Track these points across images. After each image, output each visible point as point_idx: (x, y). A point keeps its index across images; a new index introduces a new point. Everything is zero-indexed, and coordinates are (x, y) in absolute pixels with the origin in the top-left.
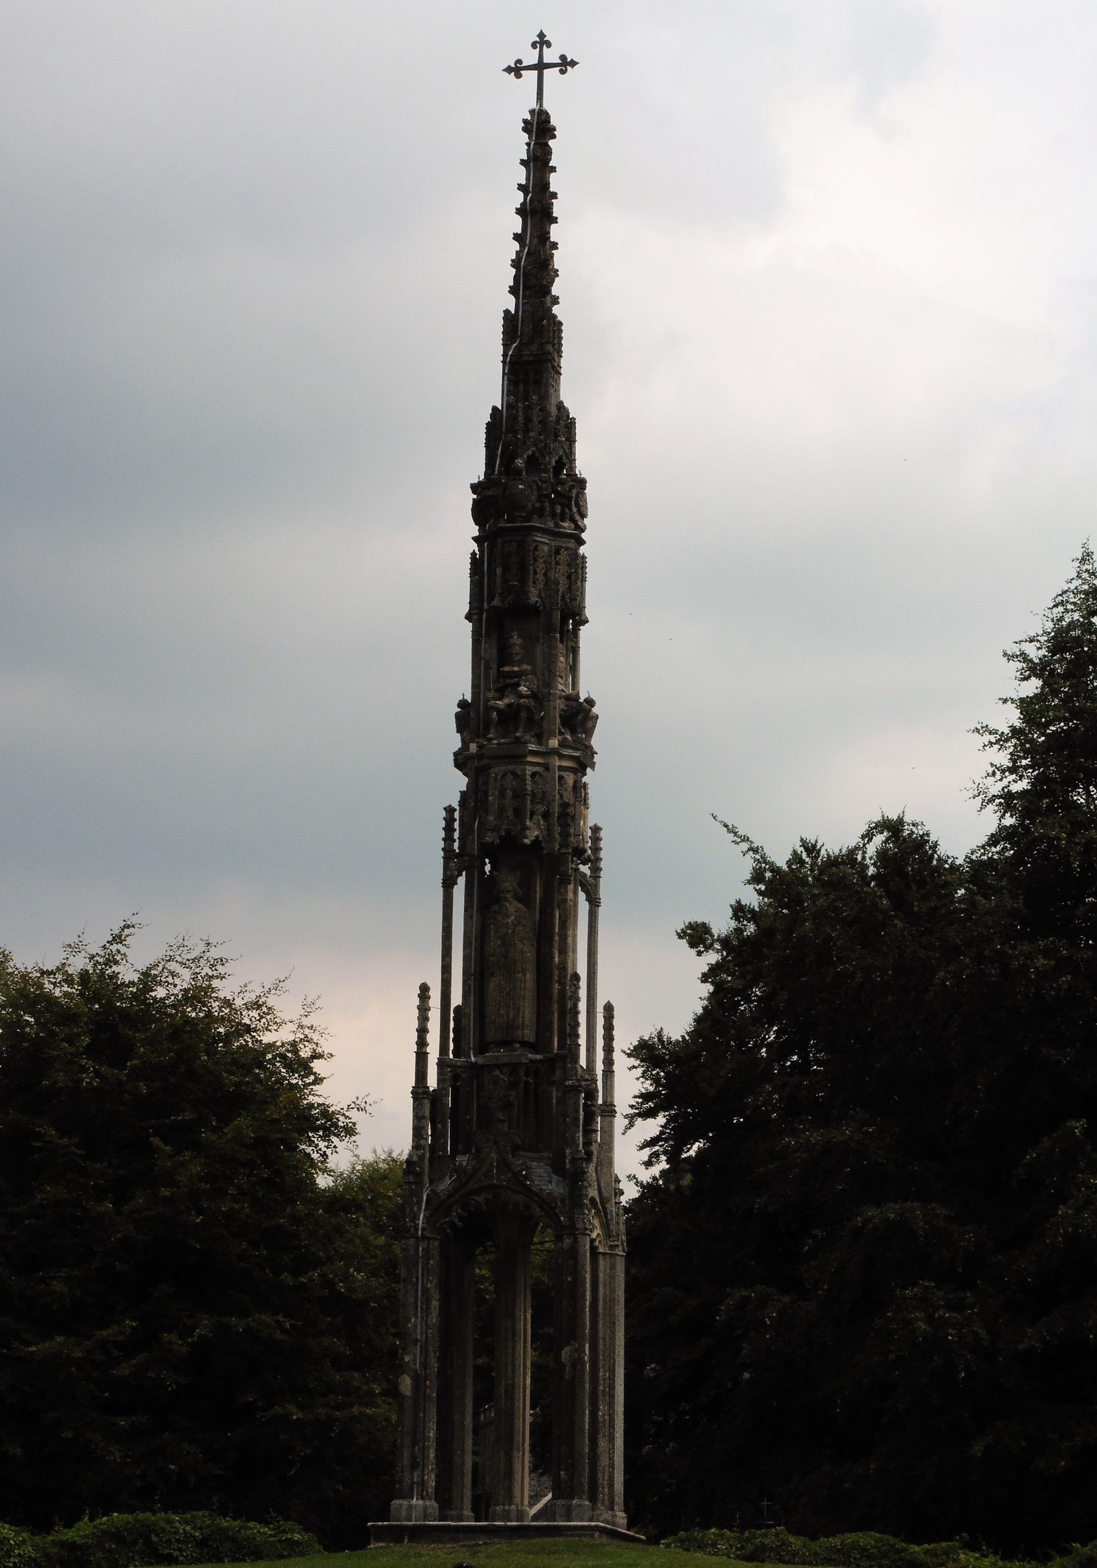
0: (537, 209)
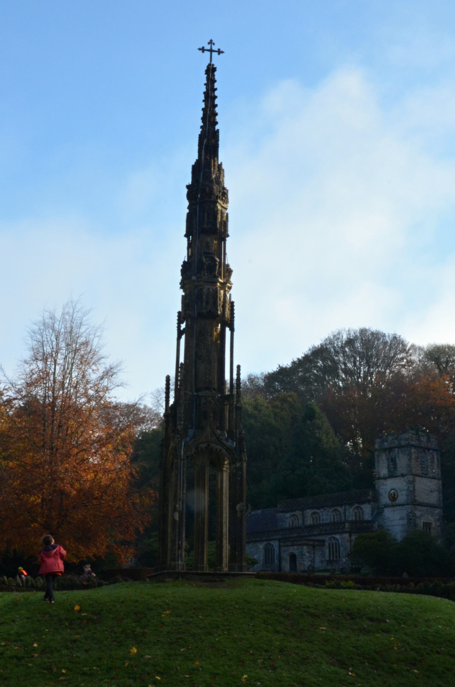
0: (210, 97)
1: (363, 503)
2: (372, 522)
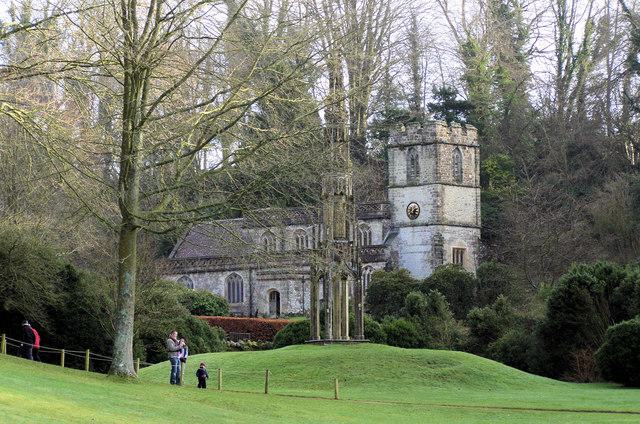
1: (371, 219)
2: (384, 246)
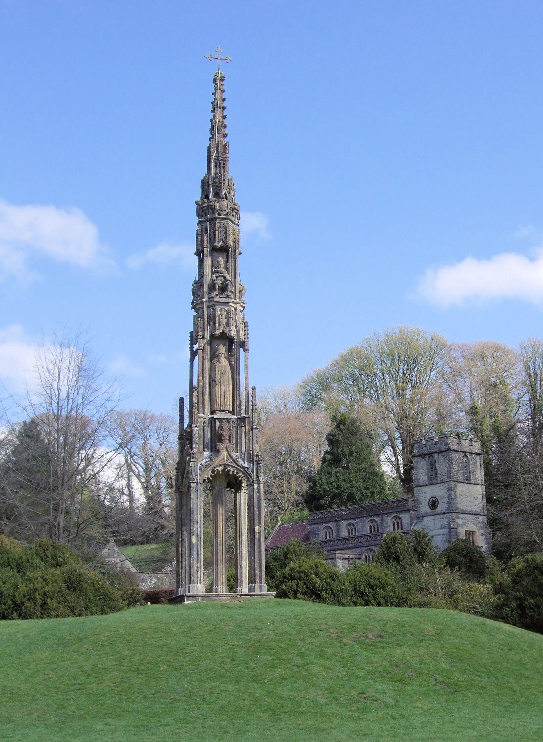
1: (402, 512)
